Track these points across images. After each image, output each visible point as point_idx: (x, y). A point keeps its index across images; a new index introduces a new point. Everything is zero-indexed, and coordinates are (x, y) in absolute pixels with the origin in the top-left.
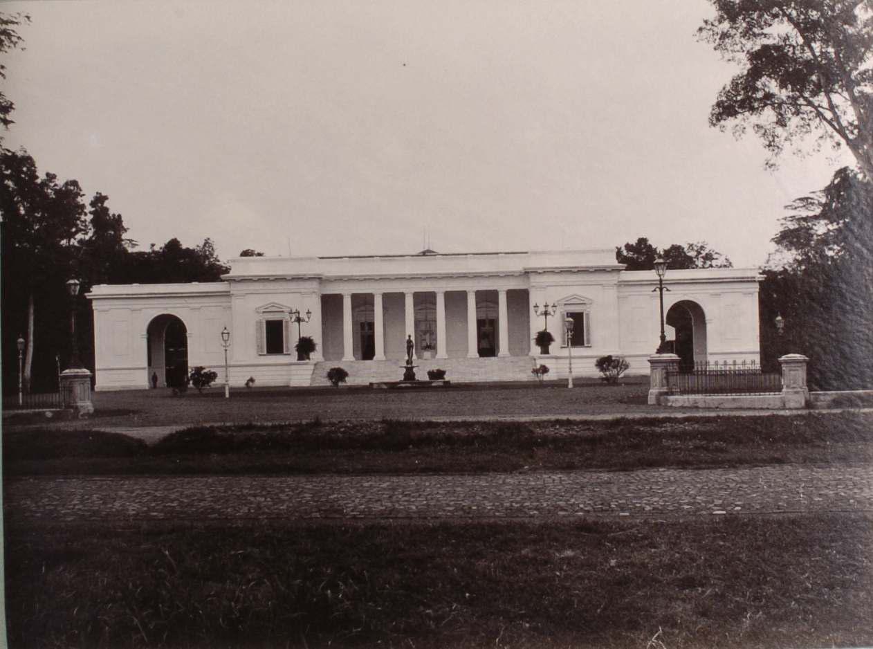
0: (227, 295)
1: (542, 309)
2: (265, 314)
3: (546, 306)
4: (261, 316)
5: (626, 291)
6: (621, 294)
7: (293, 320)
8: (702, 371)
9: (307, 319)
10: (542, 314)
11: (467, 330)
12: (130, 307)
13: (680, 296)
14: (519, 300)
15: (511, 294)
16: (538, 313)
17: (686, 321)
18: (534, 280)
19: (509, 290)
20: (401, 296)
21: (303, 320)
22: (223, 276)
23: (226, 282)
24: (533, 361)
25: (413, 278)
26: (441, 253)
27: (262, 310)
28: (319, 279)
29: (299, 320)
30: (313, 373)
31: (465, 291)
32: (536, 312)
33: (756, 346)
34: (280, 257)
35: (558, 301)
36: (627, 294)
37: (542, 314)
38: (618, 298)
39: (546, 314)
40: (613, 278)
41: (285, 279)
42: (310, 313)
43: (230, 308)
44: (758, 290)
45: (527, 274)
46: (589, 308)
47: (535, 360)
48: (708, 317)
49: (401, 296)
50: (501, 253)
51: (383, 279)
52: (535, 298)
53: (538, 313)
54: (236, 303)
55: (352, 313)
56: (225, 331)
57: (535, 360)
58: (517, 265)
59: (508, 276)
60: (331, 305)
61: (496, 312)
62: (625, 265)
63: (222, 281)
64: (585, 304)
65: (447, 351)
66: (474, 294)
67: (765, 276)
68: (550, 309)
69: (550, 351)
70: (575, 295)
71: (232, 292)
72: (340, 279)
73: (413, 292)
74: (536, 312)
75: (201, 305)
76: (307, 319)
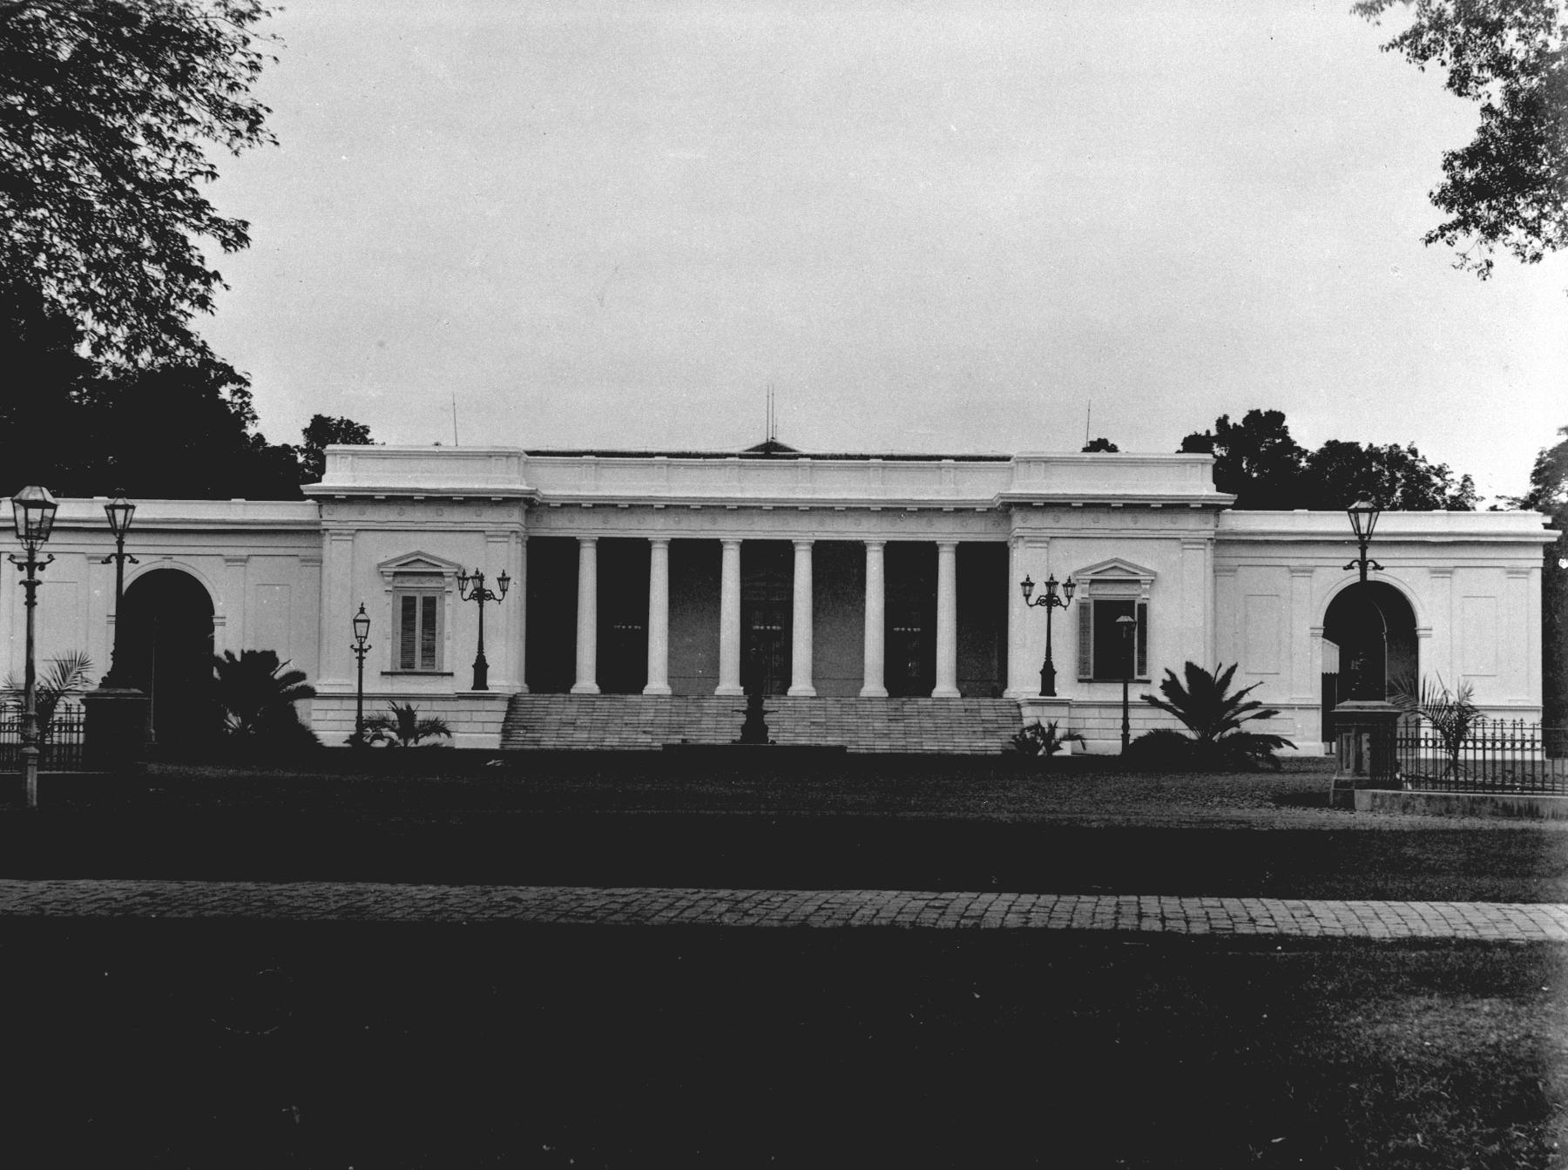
0: (313, 532)
1: (1040, 590)
2: (399, 579)
3: (1051, 584)
4: (388, 583)
5: (1233, 556)
6: (1222, 561)
7: (466, 595)
8: (1475, 748)
9: (498, 594)
10: (1039, 602)
11: (717, 629)
12: (1285, 562)
13: (155, 558)
14: (985, 570)
15: (964, 552)
16: (1032, 600)
17: (1373, 630)
18: (1019, 522)
19: (961, 543)
20: (857, 551)
21: (491, 596)
22: (307, 489)
23: (309, 501)
24: (1015, 711)
25: (893, 510)
26: (805, 452)
27: (1089, 576)
28: (531, 505)
29: (481, 595)
30: (507, 720)
31: (790, 541)
32: (1027, 596)
33: (1534, 696)
34: (437, 449)
35: (1077, 573)
36: (1235, 562)
37: (1039, 602)
38: (1216, 571)
39: (1050, 601)
40: (1200, 526)
41: (615, 506)
42: (1032, 585)
43: (320, 561)
44: (1540, 564)
45: (1008, 508)
46: (1145, 591)
47: (1019, 706)
48: (1422, 621)
49: (716, 547)
50: (733, 455)
51: (744, 509)
52: (1025, 564)
53: (1032, 600)
54: (334, 551)
55: (588, 577)
56: (362, 617)
57: (1019, 706)
58: (983, 488)
59: (962, 511)
60: (549, 565)
61: (946, 586)
62: (1235, 497)
63: (302, 497)
64: (1138, 581)
65: (814, 678)
66: (880, 548)
67: (1559, 533)
68: (1060, 592)
69: (489, 682)
70: (419, 553)
71: (325, 525)
72: (571, 506)
73: (813, 539)
74: (1027, 596)
75: (251, 551)
76: (498, 594)
